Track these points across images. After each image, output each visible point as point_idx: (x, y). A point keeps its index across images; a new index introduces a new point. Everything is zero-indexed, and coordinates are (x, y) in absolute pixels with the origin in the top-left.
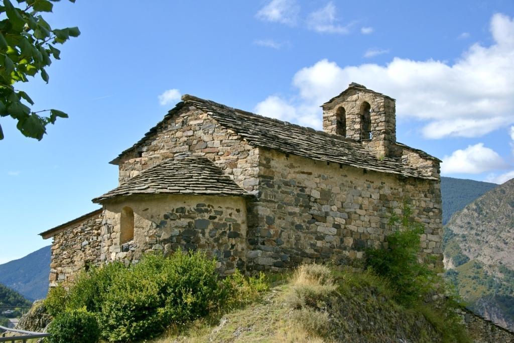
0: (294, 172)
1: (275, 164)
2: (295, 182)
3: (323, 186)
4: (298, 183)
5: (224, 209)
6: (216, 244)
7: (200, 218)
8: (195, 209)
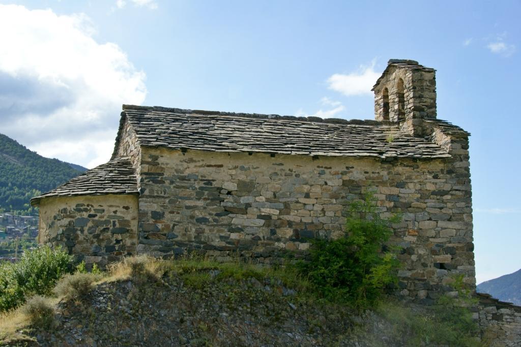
0: (196, 166)
1: (166, 160)
2: (198, 176)
3: (242, 177)
4: (202, 176)
5: (105, 208)
6: (95, 240)
7: (80, 217)
8: (74, 209)
